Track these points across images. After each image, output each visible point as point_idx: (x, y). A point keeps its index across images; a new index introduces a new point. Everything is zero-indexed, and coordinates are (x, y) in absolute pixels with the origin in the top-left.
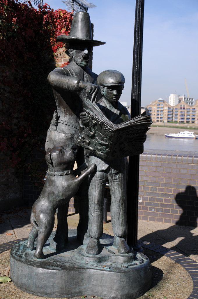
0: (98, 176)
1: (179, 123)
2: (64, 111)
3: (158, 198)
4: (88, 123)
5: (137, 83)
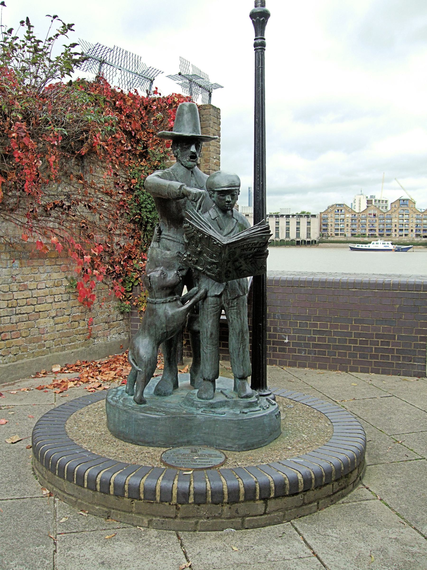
0: (210, 303)
1: (368, 237)
2: (168, 223)
4: (193, 236)
5: (259, 186)
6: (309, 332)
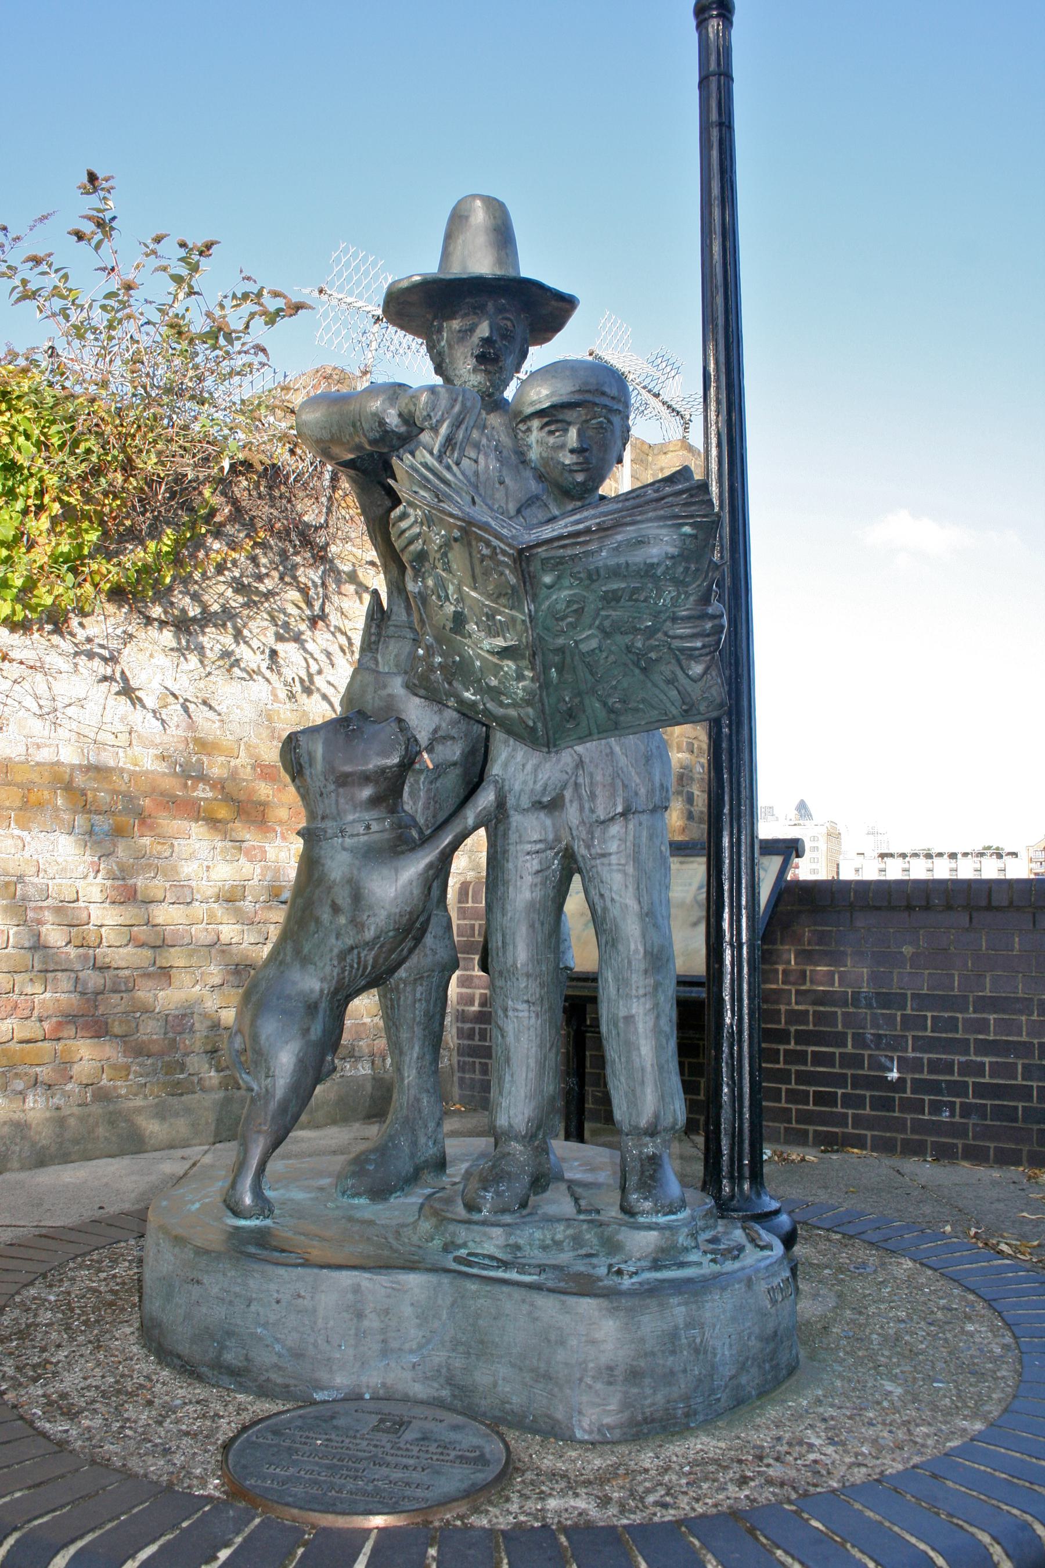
3: (963, 1059)
6: (962, 1046)
